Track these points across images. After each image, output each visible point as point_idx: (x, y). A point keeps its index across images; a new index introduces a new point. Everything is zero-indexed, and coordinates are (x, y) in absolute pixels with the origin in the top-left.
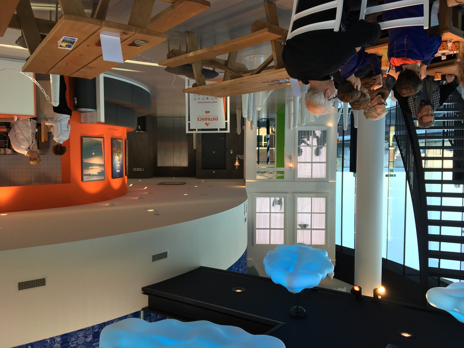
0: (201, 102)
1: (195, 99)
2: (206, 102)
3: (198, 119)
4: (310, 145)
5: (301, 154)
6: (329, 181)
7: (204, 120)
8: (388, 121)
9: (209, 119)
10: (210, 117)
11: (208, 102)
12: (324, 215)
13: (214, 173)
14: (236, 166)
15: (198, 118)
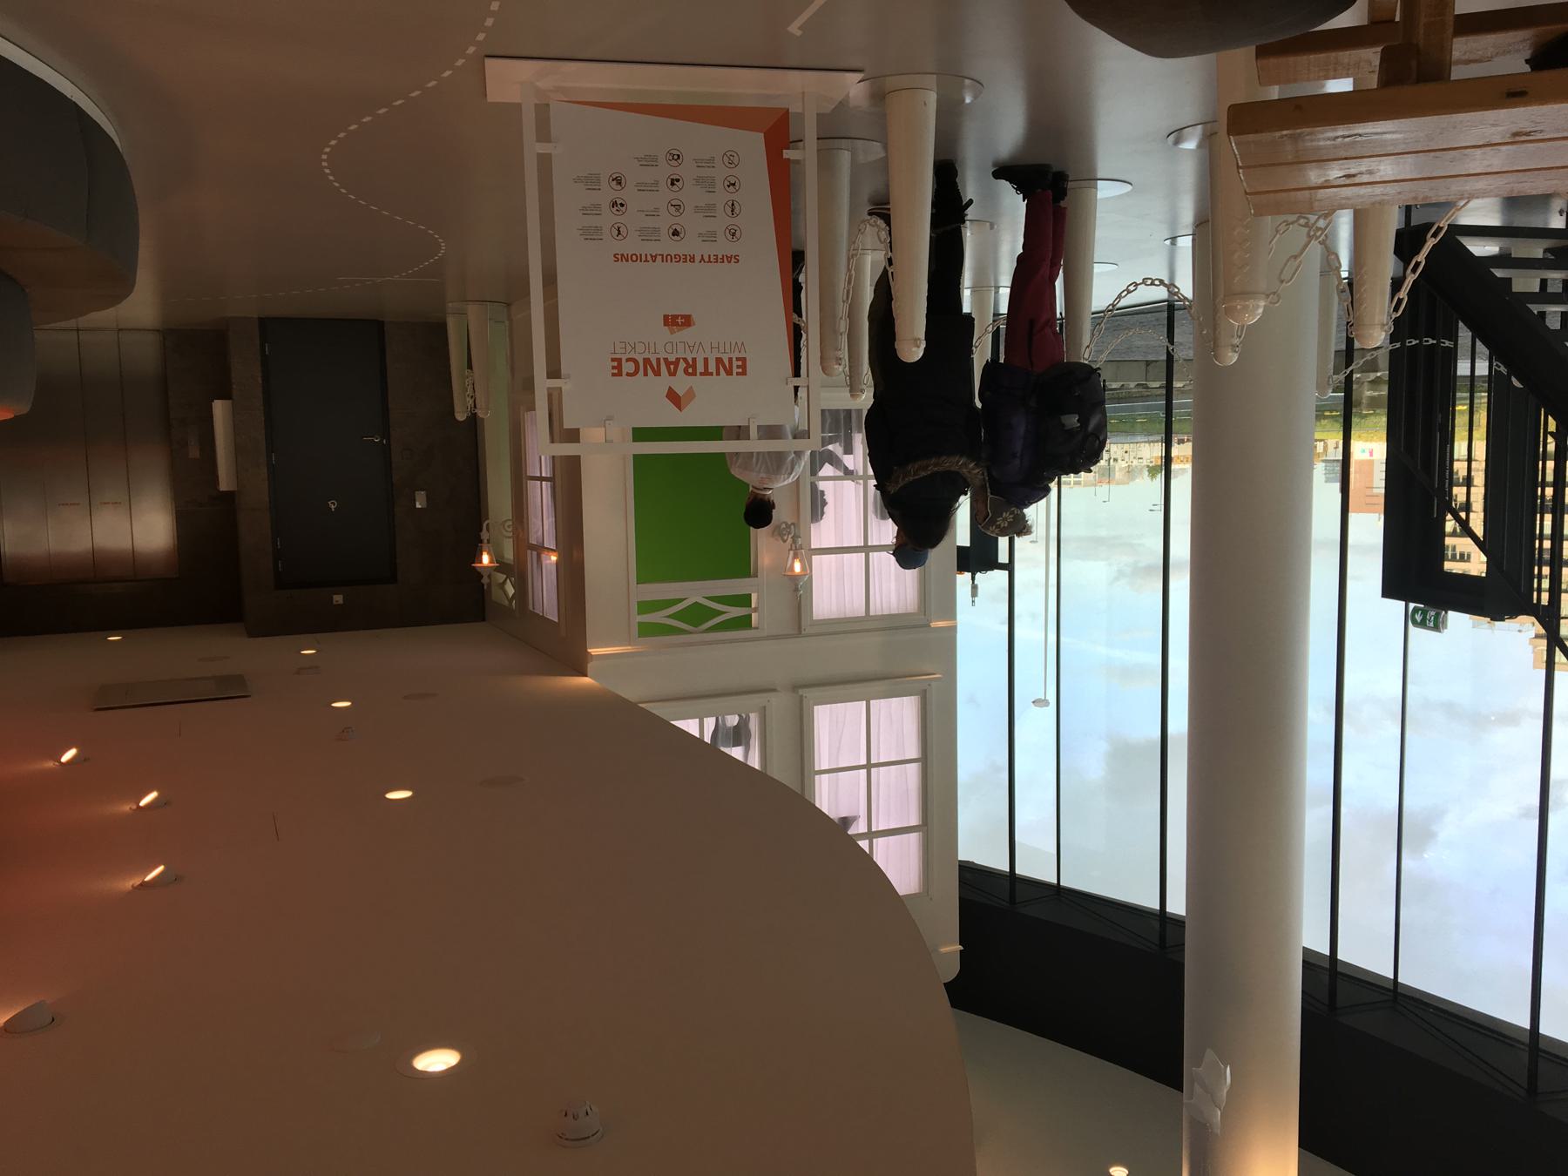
0: (635, 258)
1: (591, 234)
2: (666, 258)
3: (619, 367)
4: (855, 474)
5: (823, 513)
6: (933, 625)
7: (657, 373)
8: (1465, 399)
9: (691, 368)
10: (694, 355)
11: (678, 258)
12: (913, 770)
13: (341, 602)
14: (479, 573)
15: (619, 361)
